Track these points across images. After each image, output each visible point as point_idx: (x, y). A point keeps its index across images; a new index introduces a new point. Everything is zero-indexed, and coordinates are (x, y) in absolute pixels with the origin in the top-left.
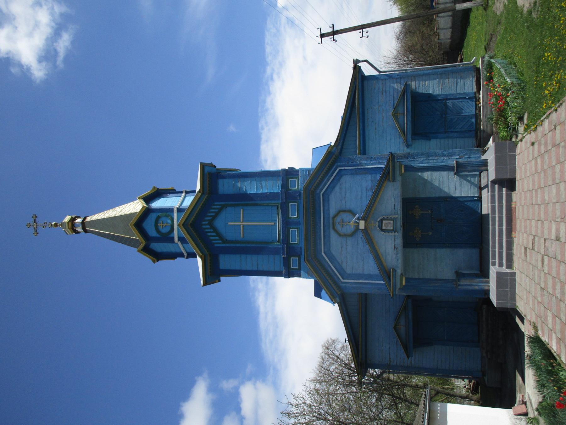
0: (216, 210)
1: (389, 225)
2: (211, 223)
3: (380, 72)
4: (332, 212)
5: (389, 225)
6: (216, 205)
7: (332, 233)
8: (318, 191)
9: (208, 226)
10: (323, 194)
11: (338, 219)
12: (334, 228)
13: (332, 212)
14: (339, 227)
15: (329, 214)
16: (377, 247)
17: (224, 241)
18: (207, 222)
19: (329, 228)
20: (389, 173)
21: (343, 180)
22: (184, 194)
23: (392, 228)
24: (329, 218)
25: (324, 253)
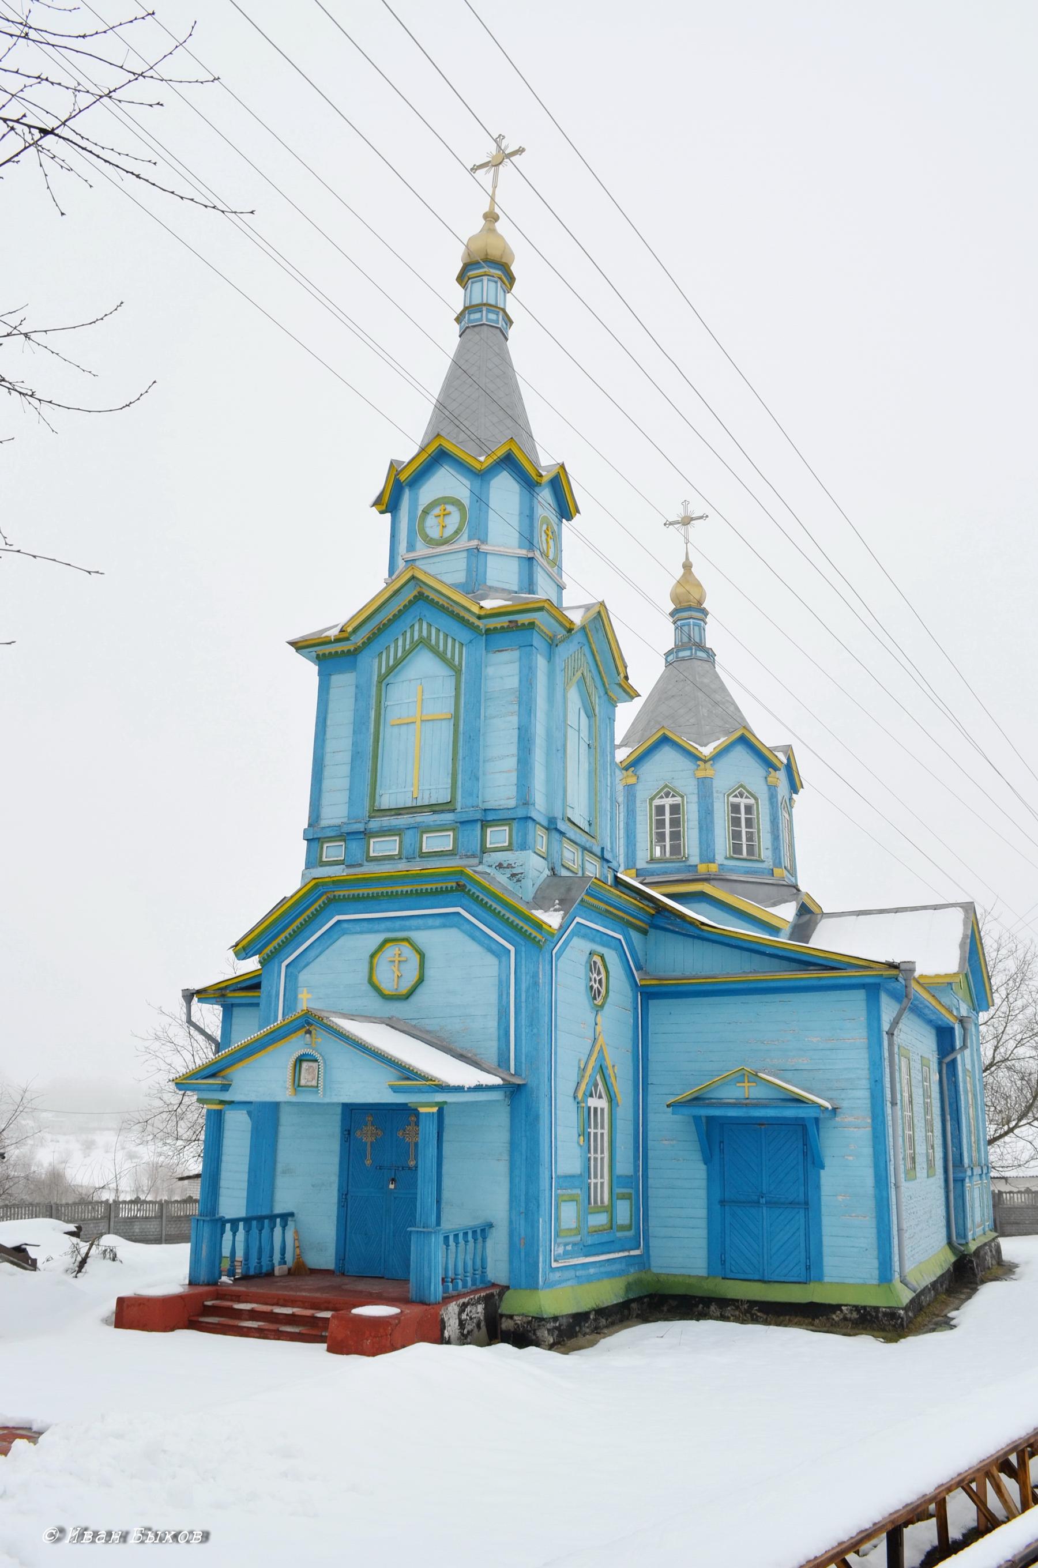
0: (449, 655)
1: (310, 1077)
2: (423, 642)
3: (890, 1034)
4: (421, 937)
5: (310, 1077)
6: (461, 653)
7: (377, 939)
8: (465, 901)
9: (416, 637)
10: (458, 913)
11: (406, 950)
12: (386, 941)
13: (421, 937)
14: (391, 951)
15: (418, 929)
16: (270, 1048)
17: (384, 680)
18: (425, 633)
19: (388, 930)
20: (408, 1079)
21: (491, 960)
22: (523, 552)
23: (303, 1082)
24: (410, 929)
25: (339, 921)
